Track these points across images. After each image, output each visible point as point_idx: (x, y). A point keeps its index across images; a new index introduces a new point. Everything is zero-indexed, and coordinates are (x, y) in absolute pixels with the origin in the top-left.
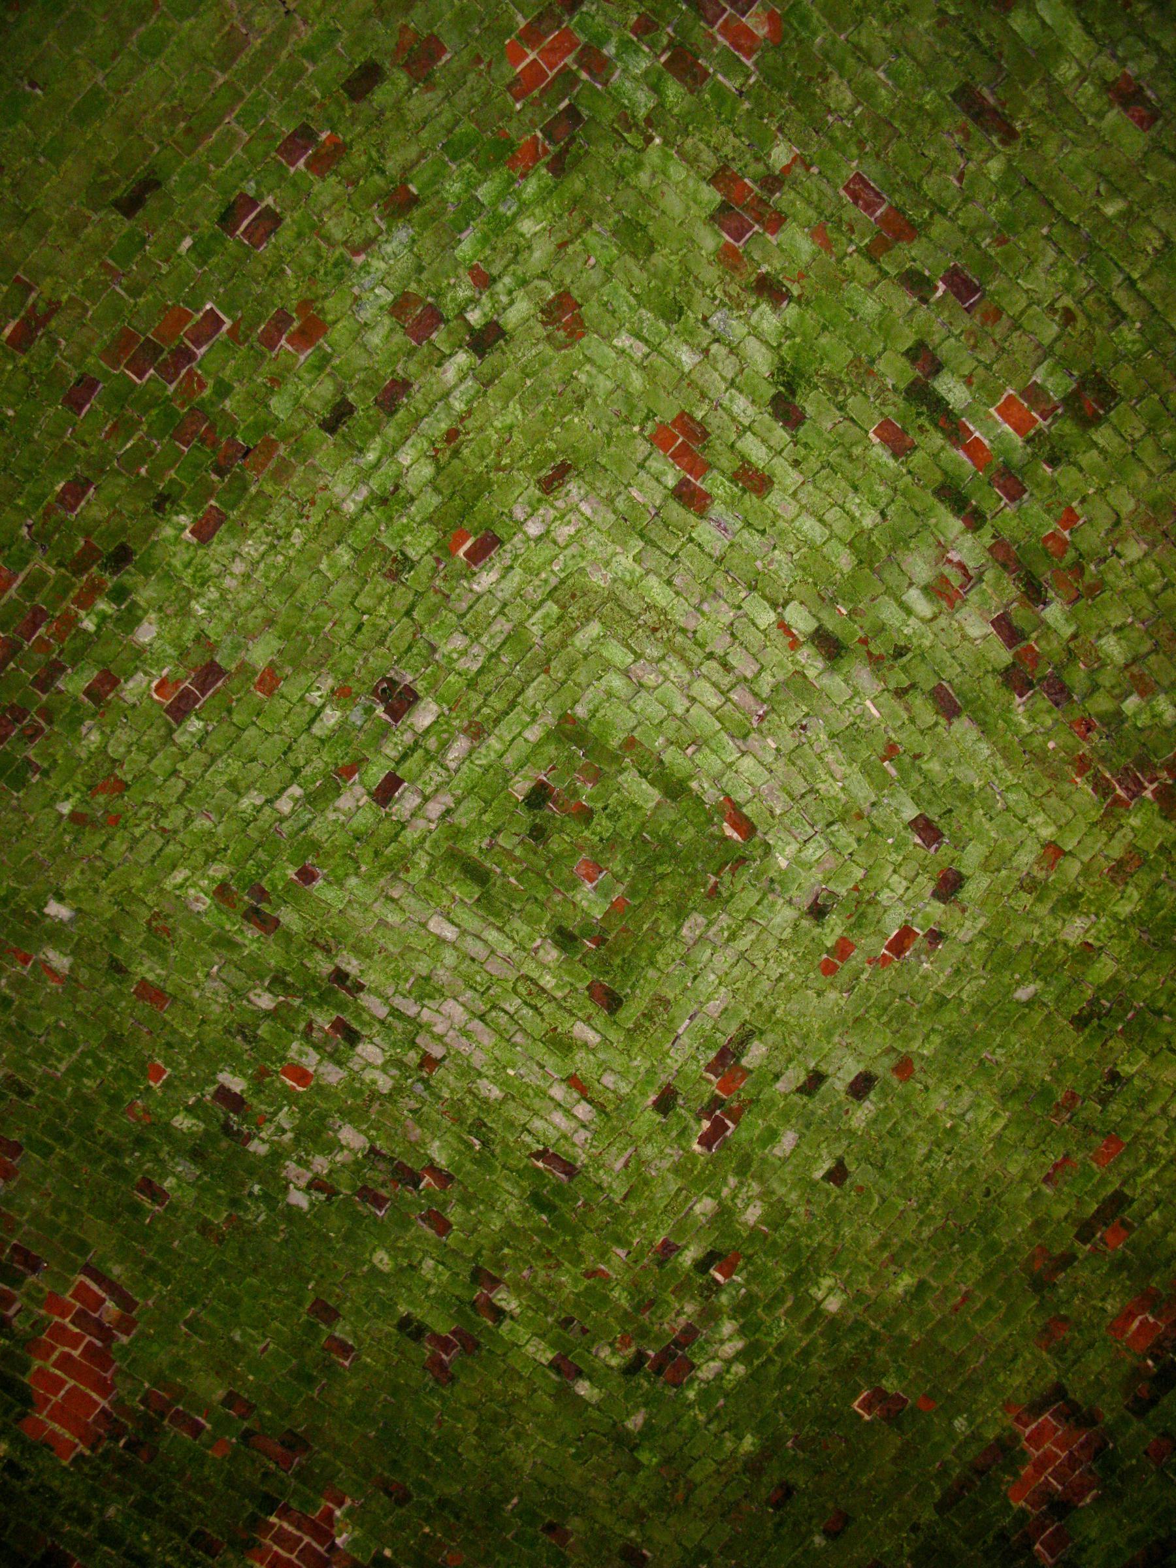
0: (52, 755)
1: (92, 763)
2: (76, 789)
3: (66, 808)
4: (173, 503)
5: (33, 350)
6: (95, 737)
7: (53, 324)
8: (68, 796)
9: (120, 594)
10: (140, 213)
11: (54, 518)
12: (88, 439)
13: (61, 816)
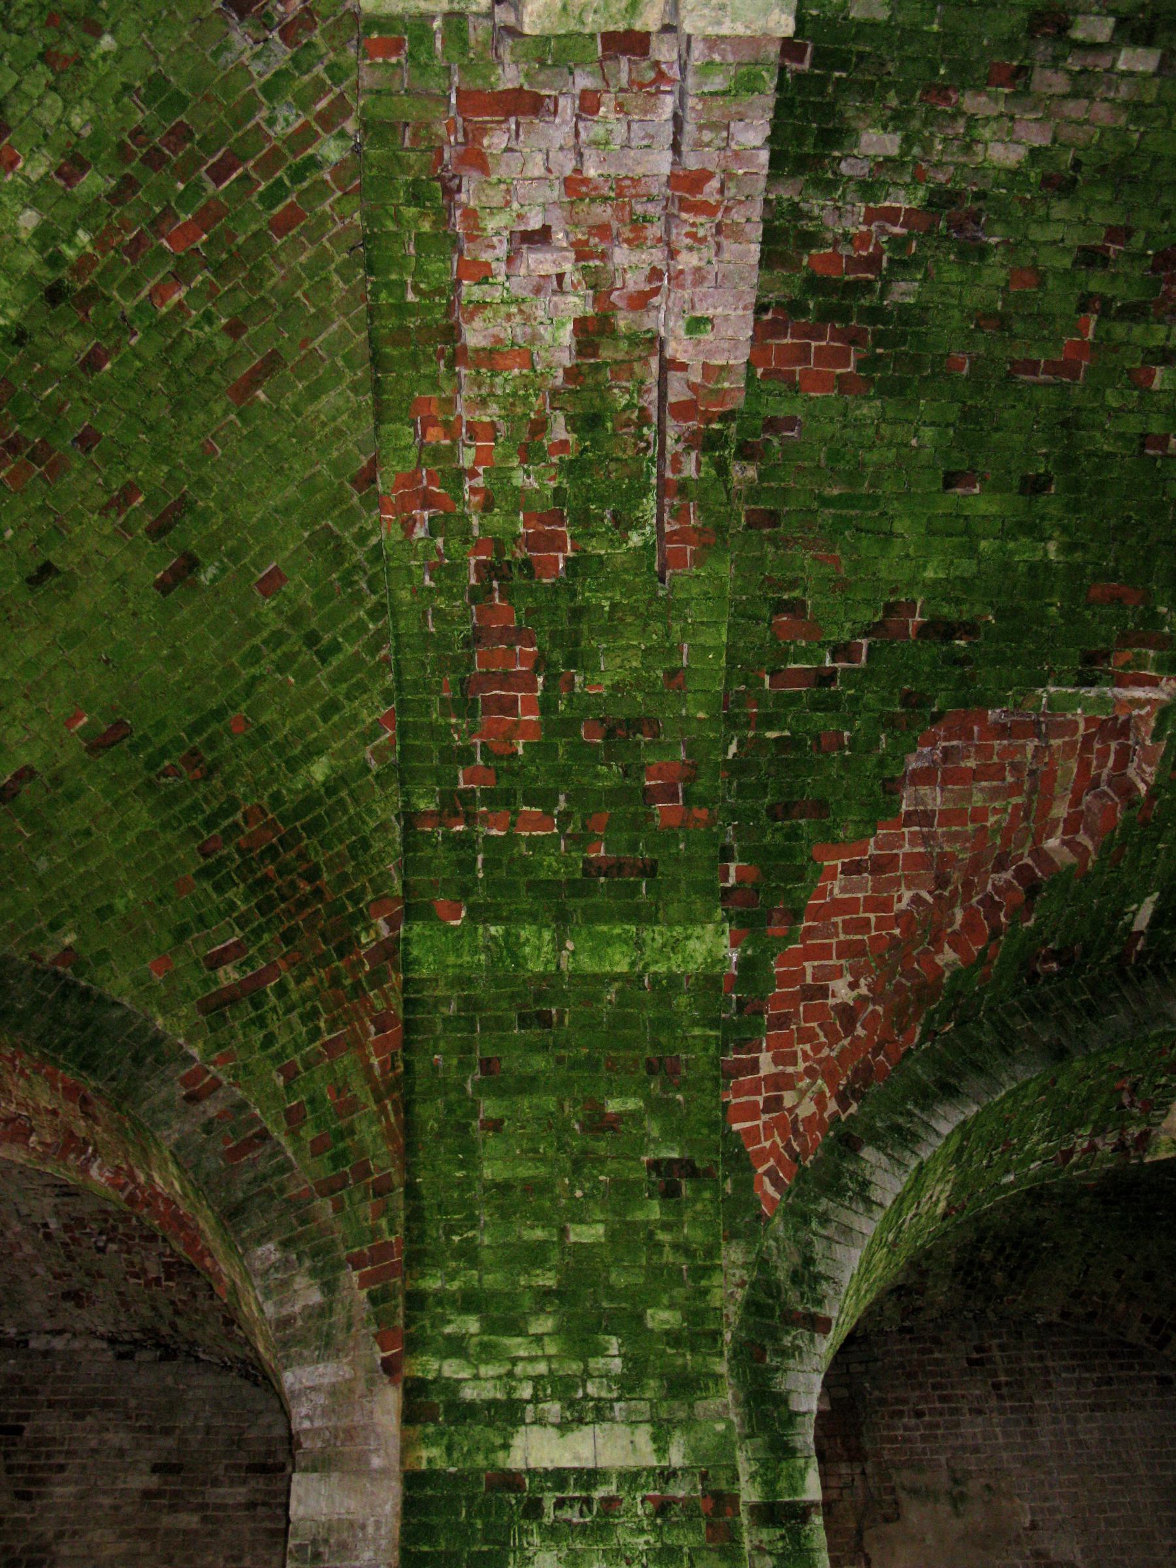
0: (118, 109)
1: (78, 93)
2: (95, 64)
3: (107, 42)
4: (9, 337)
5: (121, 483)
6: (76, 121)
7: (106, 499)
8: (104, 57)
9: (55, 261)
10: (40, 563)
11: (112, 343)
12: (81, 405)
13: (113, 32)
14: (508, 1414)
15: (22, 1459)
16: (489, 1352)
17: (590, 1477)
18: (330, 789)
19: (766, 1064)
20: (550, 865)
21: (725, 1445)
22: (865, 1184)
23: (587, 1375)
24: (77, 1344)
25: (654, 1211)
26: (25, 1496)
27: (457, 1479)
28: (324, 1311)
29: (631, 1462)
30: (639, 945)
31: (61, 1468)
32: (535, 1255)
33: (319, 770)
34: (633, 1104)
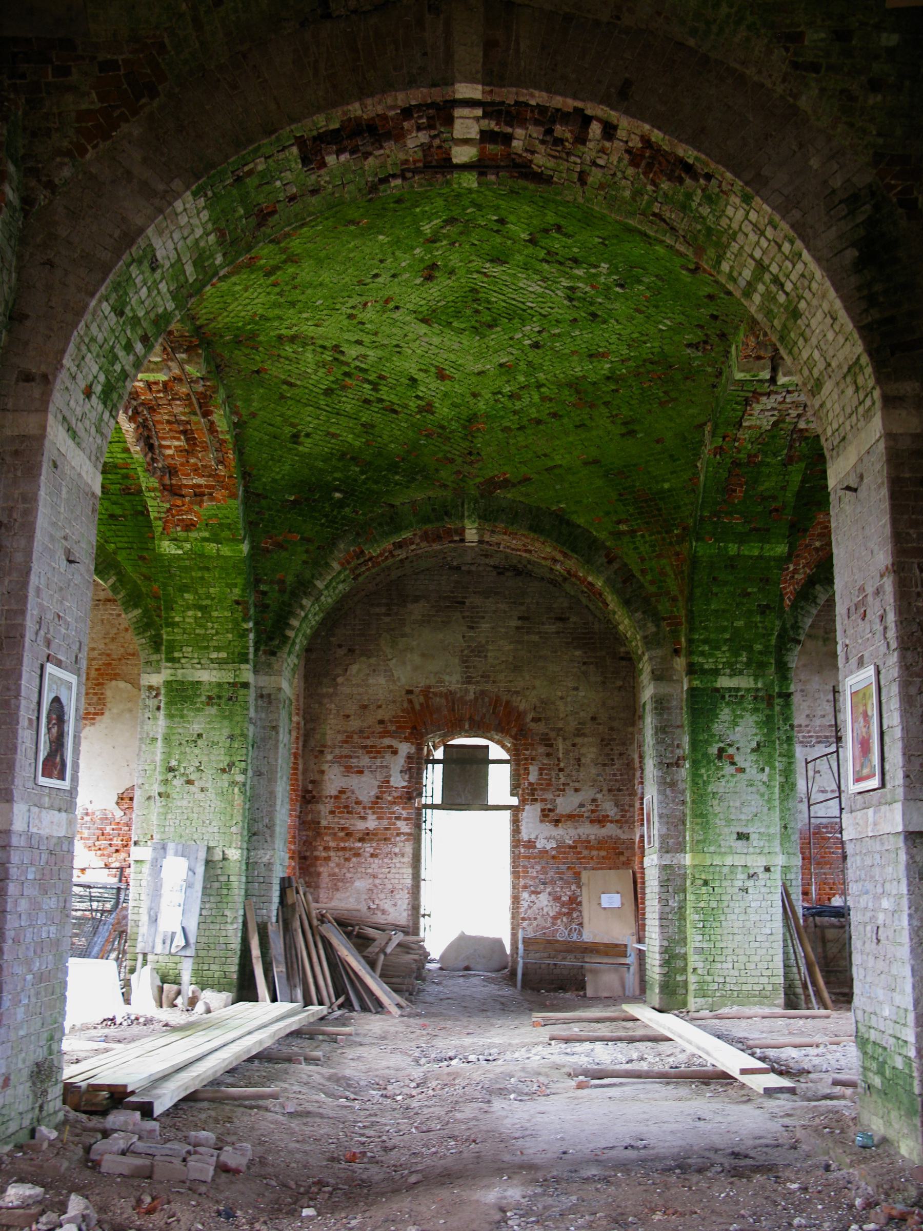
14: (716, 672)
15: (467, 614)
16: (711, 655)
17: (738, 690)
18: (669, 490)
19: (791, 567)
20: (740, 529)
21: (773, 682)
22: (816, 597)
23: (736, 662)
24: (481, 569)
25: (758, 618)
26: (472, 628)
27: (704, 689)
28: (657, 633)
29: (748, 686)
30: (762, 548)
31: (483, 617)
32: (724, 629)
33: (666, 486)
34: (755, 590)
